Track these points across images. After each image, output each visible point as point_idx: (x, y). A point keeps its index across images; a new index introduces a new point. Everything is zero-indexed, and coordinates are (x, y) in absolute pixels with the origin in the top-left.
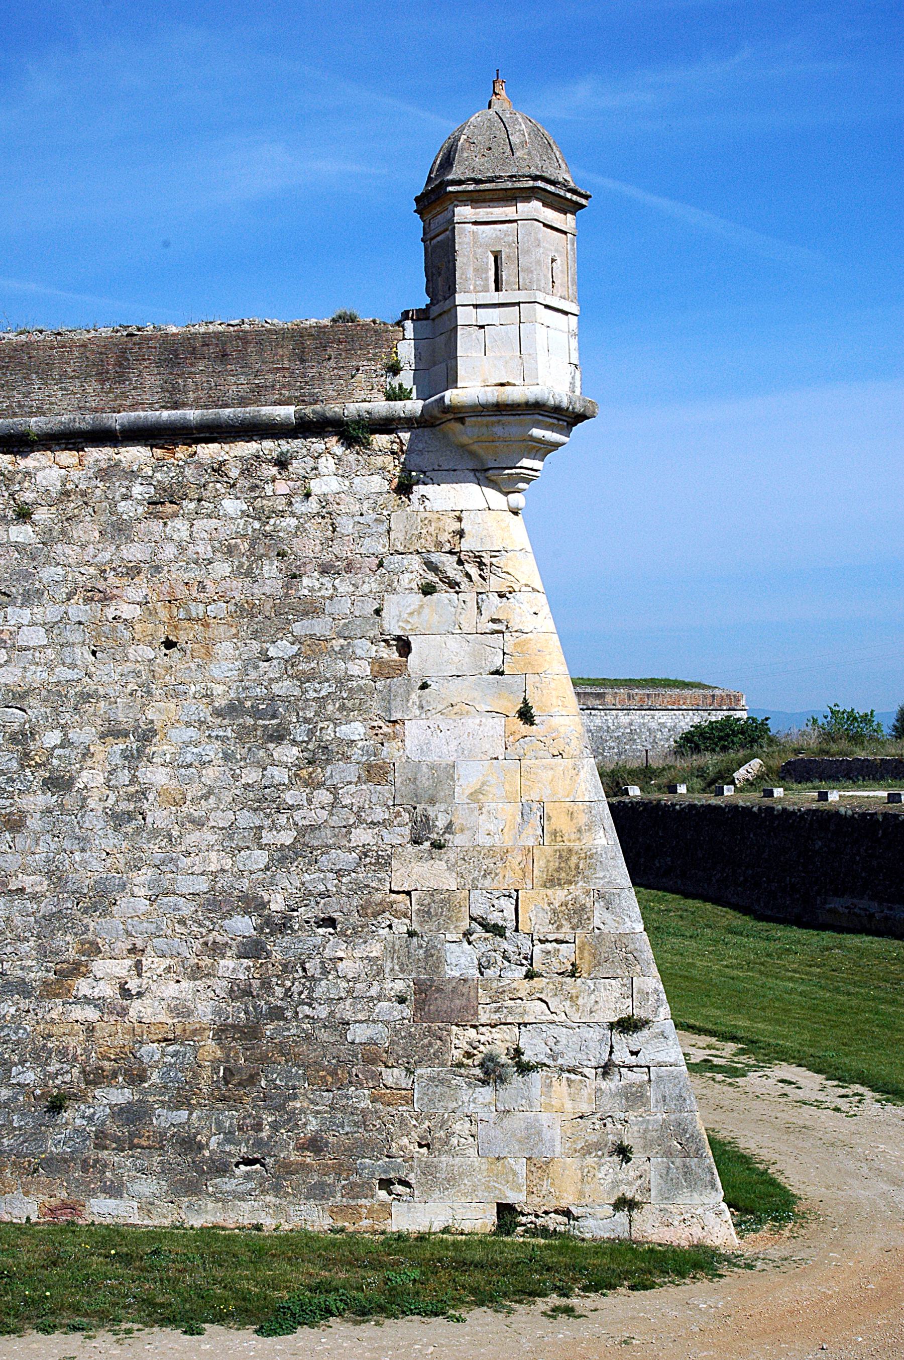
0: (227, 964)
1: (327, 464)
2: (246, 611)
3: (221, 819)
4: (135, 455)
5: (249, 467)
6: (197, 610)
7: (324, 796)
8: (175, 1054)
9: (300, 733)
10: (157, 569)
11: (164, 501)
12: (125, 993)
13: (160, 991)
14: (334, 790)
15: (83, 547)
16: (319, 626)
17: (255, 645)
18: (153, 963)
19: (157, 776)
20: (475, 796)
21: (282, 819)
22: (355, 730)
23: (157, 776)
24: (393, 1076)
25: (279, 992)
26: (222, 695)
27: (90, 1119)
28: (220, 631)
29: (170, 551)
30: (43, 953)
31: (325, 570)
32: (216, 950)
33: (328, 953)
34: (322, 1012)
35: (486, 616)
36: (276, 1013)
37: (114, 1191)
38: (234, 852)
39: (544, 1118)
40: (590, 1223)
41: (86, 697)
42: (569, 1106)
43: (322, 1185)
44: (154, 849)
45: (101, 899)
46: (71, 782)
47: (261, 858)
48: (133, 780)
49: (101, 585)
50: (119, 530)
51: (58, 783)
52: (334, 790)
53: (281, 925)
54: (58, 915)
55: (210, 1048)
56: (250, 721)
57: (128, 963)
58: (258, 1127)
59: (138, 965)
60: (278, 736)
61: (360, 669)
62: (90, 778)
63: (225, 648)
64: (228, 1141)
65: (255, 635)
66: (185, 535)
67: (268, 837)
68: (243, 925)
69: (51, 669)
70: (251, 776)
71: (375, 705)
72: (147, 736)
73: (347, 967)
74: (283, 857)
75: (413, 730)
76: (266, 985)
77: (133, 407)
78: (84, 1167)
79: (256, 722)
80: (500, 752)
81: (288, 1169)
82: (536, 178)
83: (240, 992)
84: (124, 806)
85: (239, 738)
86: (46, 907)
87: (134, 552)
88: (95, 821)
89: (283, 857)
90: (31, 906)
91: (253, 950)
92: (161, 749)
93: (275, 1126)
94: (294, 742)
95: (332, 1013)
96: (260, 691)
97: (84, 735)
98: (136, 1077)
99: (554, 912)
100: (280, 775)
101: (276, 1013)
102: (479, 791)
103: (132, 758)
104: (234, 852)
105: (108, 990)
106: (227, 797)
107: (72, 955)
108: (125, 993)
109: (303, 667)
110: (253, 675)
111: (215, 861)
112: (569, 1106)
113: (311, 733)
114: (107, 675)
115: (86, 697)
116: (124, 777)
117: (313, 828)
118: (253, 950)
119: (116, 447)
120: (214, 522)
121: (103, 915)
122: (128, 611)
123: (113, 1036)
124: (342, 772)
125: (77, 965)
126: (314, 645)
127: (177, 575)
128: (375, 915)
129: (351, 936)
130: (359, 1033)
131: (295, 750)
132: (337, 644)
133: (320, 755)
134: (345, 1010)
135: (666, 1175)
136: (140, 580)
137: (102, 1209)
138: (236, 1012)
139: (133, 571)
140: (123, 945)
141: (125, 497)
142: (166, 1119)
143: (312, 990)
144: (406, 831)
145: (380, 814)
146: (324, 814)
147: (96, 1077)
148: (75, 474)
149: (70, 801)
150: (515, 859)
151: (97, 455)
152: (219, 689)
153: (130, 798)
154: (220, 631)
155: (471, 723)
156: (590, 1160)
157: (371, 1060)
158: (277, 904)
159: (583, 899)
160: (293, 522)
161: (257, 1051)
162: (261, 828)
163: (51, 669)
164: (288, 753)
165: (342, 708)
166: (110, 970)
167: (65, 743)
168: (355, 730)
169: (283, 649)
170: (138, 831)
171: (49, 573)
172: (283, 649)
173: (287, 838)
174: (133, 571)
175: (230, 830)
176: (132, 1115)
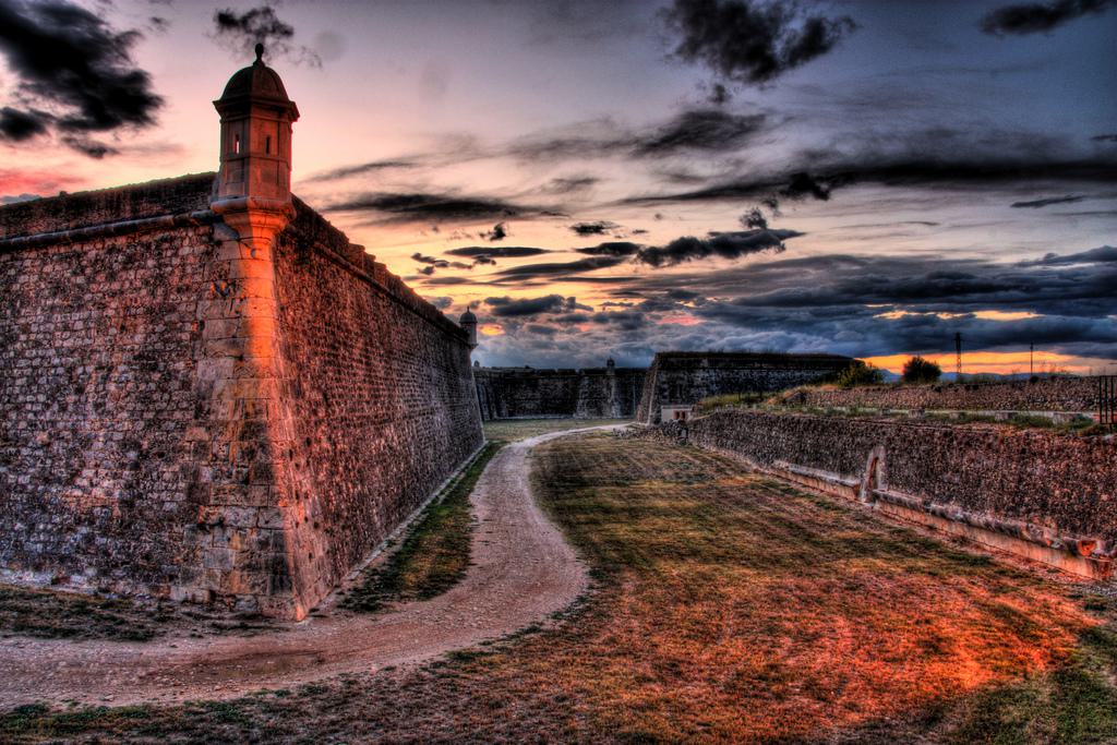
2: (150, 311)
3: (131, 406)
4: (121, 241)
5: (159, 244)
7: (166, 396)
12: (92, 485)
14: (170, 393)
15: (100, 284)
16: (174, 317)
20: (219, 396)
21: (151, 407)
22: (181, 365)
23: (112, 387)
28: (140, 320)
29: (127, 285)
30: (68, 466)
32: (123, 466)
36: (140, 496)
39: (230, 551)
41: (92, 352)
42: (239, 546)
43: (148, 575)
47: (142, 424)
48: (104, 389)
49: (103, 302)
52: (170, 393)
54: (73, 449)
55: (117, 512)
57: (94, 471)
58: (129, 547)
59: (97, 472)
61: (185, 336)
63: (141, 328)
64: (119, 553)
65: (152, 322)
66: (133, 277)
67: (145, 415)
69: (83, 339)
71: (189, 353)
73: (167, 476)
74: (149, 425)
75: (201, 365)
77: (121, 220)
80: (231, 375)
85: (141, 370)
88: (89, 407)
91: (136, 466)
92: (115, 375)
93: (135, 548)
94: (160, 372)
95: (159, 497)
97: (90, 369)
98: (91, 523)
99: (243, 452)
100: (153, 386)
112: (239, 546)
113: (165, 367)
115: (92, 352)
116: (101, 387)
117: (162, 411)
118: (136, 466)
119: (727, 69)
121: (88, 449)
124: (175, 385)
125: (78, 471)
126: (171, 327)
128: (179, 451)
129: (169, 461)
131: (159, 375)
133: (169, 375)
134: (164, 495)
135: (273, 581)
136: (116, 299)
138: (127, 495)
140: (93, 463)
141: (116, 261)
142: (100, 541)
143: (153, 486)
144: (193, 413)
146: (165, 405)
147: (79, 522)
148: (101, 252)
149: (83, 398)
150: (231, 426)
152: (136, 347)
153: (102, 397)
154: (140, 320)
155: (222, 360)
158: (145, 444)
159: (255, 447)
162: (143, 411)
163: (83, 339)
164: (156, 376)
168: (181, 365)
169: (160, 328)
170: (103, 411)
172: (160, 328)
173: (151, 415)
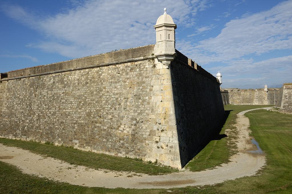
0: (133, 127)
1: (147, 64)
2: (138, 83)
4: (129, 64)
6: (133, 83)
7: (143, 106)
8: (127, 137)
9: (142, 98)
10: (130, 78)
11: (131, 70)
12: (123, 130)
13: (126, 130)
16: (144, 85)
17: (138, 87)
18: (126, 126)
19: (128, 103)
20: (158, 106)
23: (128, 103)
24: (147, 142)
25: (137, 130)
26: (135, 94)
27: (119, 144)
31: (146, 77)
32: (132, 125)
33: (142, 126)
34: (141, 133)
35: (161, 83)
36: (137, 133)
37: (121, 153)
38: (134, 113)
40: (165, 163)
44: (128, 112)
45: (122, 118)
46: (121, 104)
47: (137, 114)
49: (125, 80)
50: (127, 74)
51: (120, 104)
53: (138, 122)
55: (130, 137)
56: (137, 97)
60: (140, 99)
62: (122, 104)
65: (139, 86)
67: (138, 111)
68: (134, 122)
70: (137, 104)
72: (128, 99)
76: (136, 130)
78: (118, 150)
79: (137, 97)
81: (136, 152)
82: (165, 24)
83: (133, 130)
84: (125, 107)
86: (118, 119)
87: (128, 76)
88: (122, 109)
89: (139, 114)
90: (116, 119)
91: (135, 125)
92: (129, 100)
94: (141, 99)
96: (138, 93)
97: (122, 99)
98: (123, 140)
100: (139, 103)
101: (137, 133)
102: (158, 106)
103: (126, 101)
104: (134, 113)
105: (122, 129)
106: (134, 106)
107: (119, 125)
108: (123, 130)
109: (143, 90)
110: (138, 91)
111: (133, 114)
114: (124, 91)
116: (125, 104)
118: (135, 125)
120: (136, 72)
122: (127, 83)
123: (122, 135)
124: (145, 103)
127: (132, 79)
130: (144, 136)
131: (141, 100)
132: (146, 87)
133: (144, 101)
134: (143, 133)
137: (119, 155)
139: (128, 79)
145: (149, 109)
151: (126, 64)
155: (159, 97)
156: (166, 155)
157: (145, 140)
160: (143, 71)
161: (135, 138)
164: (140, 101)
165: (146, 95)
166: (122, 126)
167: (121, 100)
168: (147, 98)
169: (141, 88)
171: (121, 79)
172: (141, 88)
173: (139, 111)
174: (128, 79)
175: (134, 111)
176: (123, 144)
